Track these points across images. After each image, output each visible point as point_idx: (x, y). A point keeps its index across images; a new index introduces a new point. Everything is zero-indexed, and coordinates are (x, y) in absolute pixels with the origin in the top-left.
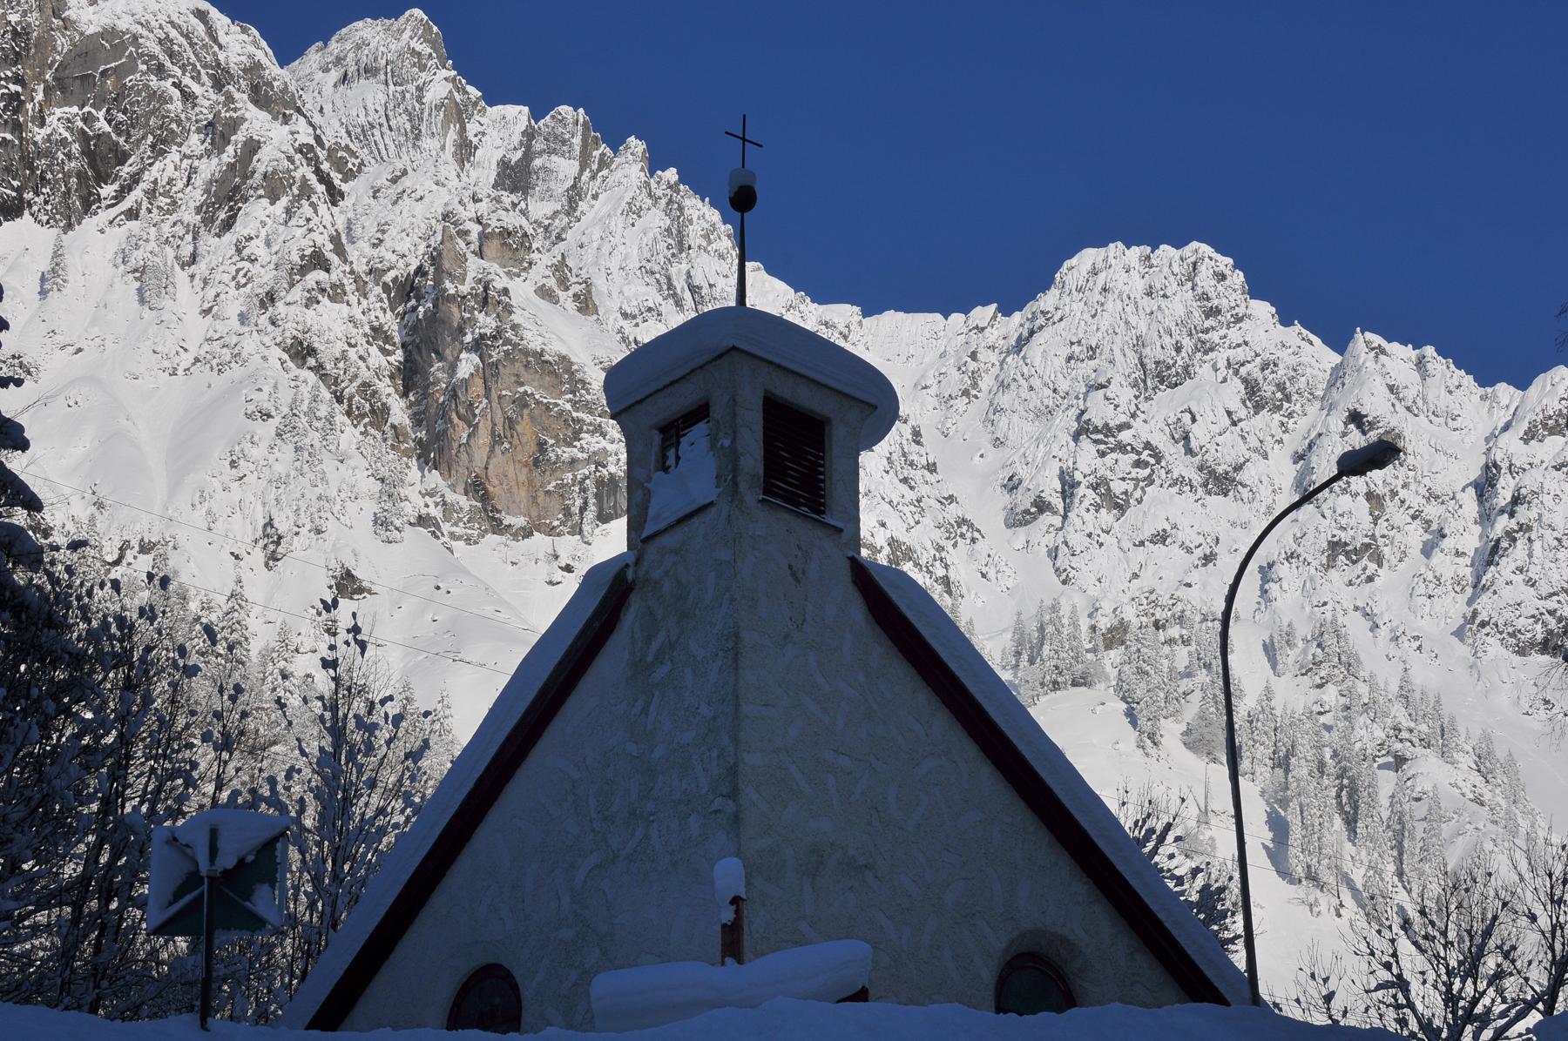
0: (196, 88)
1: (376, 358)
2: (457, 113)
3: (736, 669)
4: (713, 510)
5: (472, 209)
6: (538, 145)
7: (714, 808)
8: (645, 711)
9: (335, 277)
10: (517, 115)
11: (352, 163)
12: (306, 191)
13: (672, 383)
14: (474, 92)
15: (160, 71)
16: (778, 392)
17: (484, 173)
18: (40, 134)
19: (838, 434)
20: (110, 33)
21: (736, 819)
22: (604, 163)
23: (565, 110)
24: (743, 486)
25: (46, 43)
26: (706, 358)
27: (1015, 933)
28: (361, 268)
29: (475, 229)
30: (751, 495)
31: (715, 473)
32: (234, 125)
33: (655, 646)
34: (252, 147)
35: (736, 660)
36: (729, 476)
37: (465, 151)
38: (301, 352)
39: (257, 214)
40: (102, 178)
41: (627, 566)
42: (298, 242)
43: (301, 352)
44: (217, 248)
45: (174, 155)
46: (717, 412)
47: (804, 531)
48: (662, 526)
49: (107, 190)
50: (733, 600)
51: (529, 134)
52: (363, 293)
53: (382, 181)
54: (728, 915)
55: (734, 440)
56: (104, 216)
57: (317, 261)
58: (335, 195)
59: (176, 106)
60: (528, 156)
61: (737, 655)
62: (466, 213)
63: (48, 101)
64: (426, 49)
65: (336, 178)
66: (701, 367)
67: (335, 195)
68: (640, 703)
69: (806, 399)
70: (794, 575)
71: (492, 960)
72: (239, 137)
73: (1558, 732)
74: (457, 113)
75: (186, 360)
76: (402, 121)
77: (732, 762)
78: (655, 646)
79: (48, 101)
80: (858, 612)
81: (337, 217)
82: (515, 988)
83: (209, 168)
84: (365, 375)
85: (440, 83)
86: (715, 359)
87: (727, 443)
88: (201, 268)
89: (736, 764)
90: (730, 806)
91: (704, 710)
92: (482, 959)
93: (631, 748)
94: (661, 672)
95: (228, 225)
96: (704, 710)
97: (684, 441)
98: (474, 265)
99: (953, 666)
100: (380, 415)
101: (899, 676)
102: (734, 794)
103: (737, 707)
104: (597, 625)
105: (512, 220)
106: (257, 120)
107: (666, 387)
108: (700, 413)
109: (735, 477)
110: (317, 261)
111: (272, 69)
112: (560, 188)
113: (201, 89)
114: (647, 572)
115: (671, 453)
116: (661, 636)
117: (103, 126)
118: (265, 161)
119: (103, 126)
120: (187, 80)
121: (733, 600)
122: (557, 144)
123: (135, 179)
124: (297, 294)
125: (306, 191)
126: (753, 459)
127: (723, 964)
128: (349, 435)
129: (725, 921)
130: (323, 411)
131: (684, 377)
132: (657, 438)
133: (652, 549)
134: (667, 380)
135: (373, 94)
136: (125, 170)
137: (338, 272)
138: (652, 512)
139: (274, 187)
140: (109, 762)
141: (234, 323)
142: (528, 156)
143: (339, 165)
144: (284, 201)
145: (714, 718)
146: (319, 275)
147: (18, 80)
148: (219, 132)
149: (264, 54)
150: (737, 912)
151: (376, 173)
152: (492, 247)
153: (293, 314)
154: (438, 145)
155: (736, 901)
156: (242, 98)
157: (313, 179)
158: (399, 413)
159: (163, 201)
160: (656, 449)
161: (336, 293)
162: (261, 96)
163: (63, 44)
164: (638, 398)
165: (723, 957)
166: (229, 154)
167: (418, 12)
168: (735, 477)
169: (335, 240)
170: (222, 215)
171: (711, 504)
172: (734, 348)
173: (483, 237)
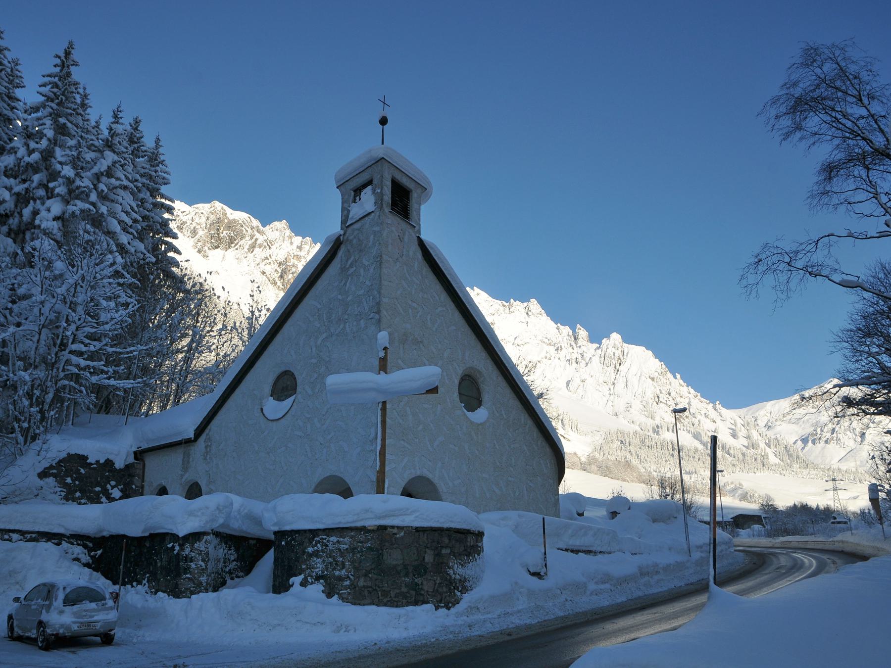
0: (248, 229)
1: (276, 275)
2: (290, 238)
3: (381, 268)
4: (373, 214)
5: (292, 251)
6: (303, 243)
7: (370, 317)
8: (345, 284)
9: (269, 261)
10: (300, 238)
11: (273, 243)
12: (265, 247)
13: (359, 173)
14: (293, 234)
15: (242, 226)
16: (397, 177)
17: (294, 246)
18: (222, 235)
19: (414, 196)
20: (234, 219)
21: (379, 321)
22: (313, 247)
23: (308, 238)
24: (384, 206)
25: (223, 220)
26: (372, 162)
27: (465, 368)
28: (274, 260)
29: (293, 255)
30: (387, 210)
31: (374, 201)
32: (254, 236)
33: (349, 262)
34: (257, 240)
35: (380, 265)
36: (379, 202)
37: (291, 243)
38: (263, 273)
39: (257, 250)
40: (232, 243)
41: (341, 235)
42: (263, 255)
43: (263, 273)
44: (250, 255)
45: (244, 240)
46: (375, 182)
47: (403, 225)
48: (354, 221)
49: (233, 245)
50: (380, 243)
51: (302, 242)
52: (274, 263)
53: (278, 246)
54: (382, 354)
55: (382, 190)
56: (232, 249)
57: (267, 258)
58: (270, 248)
59: (244, 232)
60: (302, 245)
61: (381, 263)
62: (291, 252)
63: (223, 230)
64: (286, 227)
65: (270, 245)
66: (370, 166)
67: (270, 248)
68: (343, 282)
69: (404, 181)
70: (400, 239)
71: (287, 369)
72: (255, 238)
73: (748, 292)
74: (290, 238)
75: (245, 273)
76: (281, 238)
77: (378, 300)
78: (349, 262)
79: (223, 230)
80: (419, 255)
81: (270, 252)
82: (295, 379)
83: (250, 242)
84: (274, 277)
85: (288, 232)
86: (376, 163)
87: (379, 191)
88: (247, 259)
89: (380, 301)
90: (377, 316)
91: (368, 283)
92: (283, 369)
93: (340, 297)
94: (352, 270)
95: (252, 252)
96: (368, 283)
97: (362, 193)
98: (292, 261)
99: (449, 277)
100: (276, 284)
101: (431, 278)
102: (378, 312)
103: (380, 281)
104: (329, 255)
105: (299, 253)
106: (258, 235)
107: (357, 175)
108: (370, 183)
109: (382, 202)
110: (267, 258)
111: (261, 227)
112: (306, 251)
113: (249, 230)
114: (348, 237)
115: (358, 198)
116: (352, 259)
117: (232, 235)
118: (258, 242)
119: (232, 235)
120: (246, 228)
121: (380, 243)
122: (306, 243)
123: (237, 243)
124: (264, 263)
125: (265, 247)
126: (388, 197)
127: (379, 374)
128: (271, 286)
129: (380, 356)
130: (267, 282)
131: (363, 171)
132: (353, 193)
133: (349, 230)
134: (358, 172)
135: (277, 233)
136: (236, 242)
137: (270, 260)
138: (350, 216)
139: (260, 246)
140: (457, 448)
141: (253, 268)
142: (302, 245)
143: (271, 243)
144: (262, 248)
145: (372, 285)
146: (266, 261)
147: (218, 226)
148: (252, 237)
149: (259, 225)
150: (386, 353)
151: (277, 245)
152: (295, 258)
153: (263, 267)
154: (287, 242)
155: (385, 349)
156: (255, 232)
157: (266, 245)
158: (279, 284)
159: (242, 247)
160: (352, 197)
161: (270, 264)
162: (258, 231)
163: (226, 221)
164: (347, 179)
165: (379, 371)
166: (253, 240)
167: (284, 221)
168: (382, 202)
169: (270, 255)
170: (252, 250)
171: (373, 212)
172: (383, 158)
173: (294, 256)
